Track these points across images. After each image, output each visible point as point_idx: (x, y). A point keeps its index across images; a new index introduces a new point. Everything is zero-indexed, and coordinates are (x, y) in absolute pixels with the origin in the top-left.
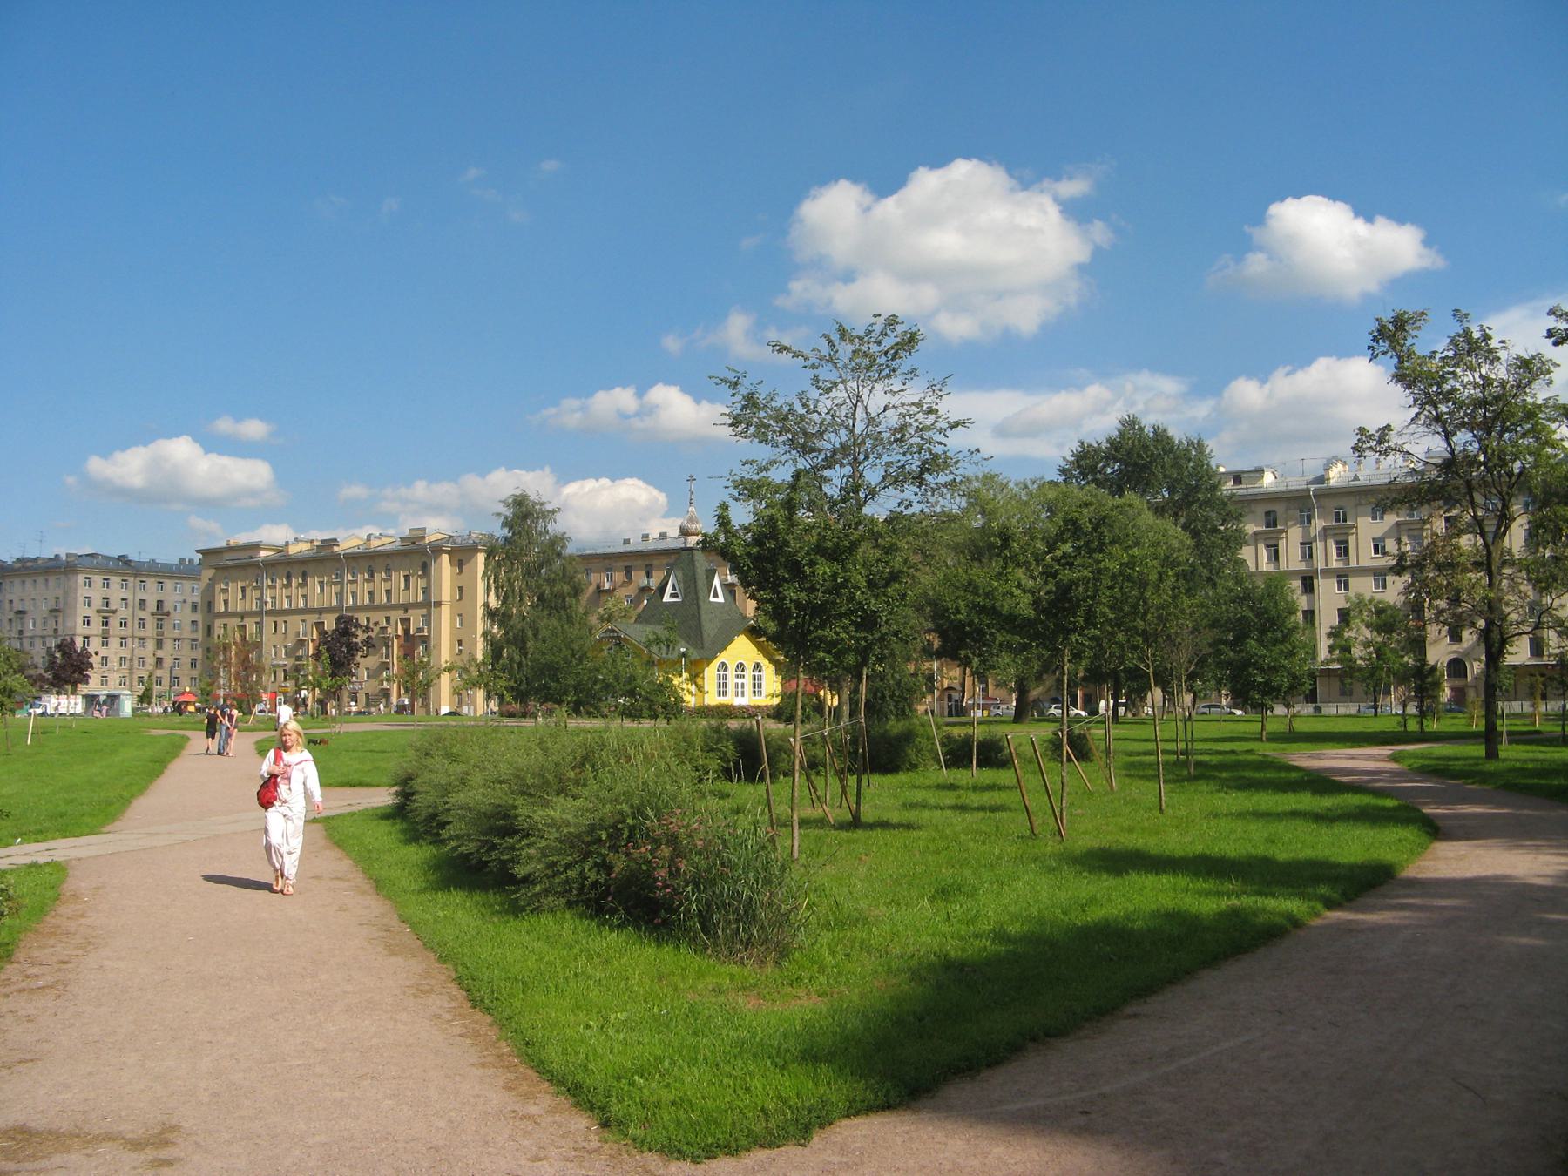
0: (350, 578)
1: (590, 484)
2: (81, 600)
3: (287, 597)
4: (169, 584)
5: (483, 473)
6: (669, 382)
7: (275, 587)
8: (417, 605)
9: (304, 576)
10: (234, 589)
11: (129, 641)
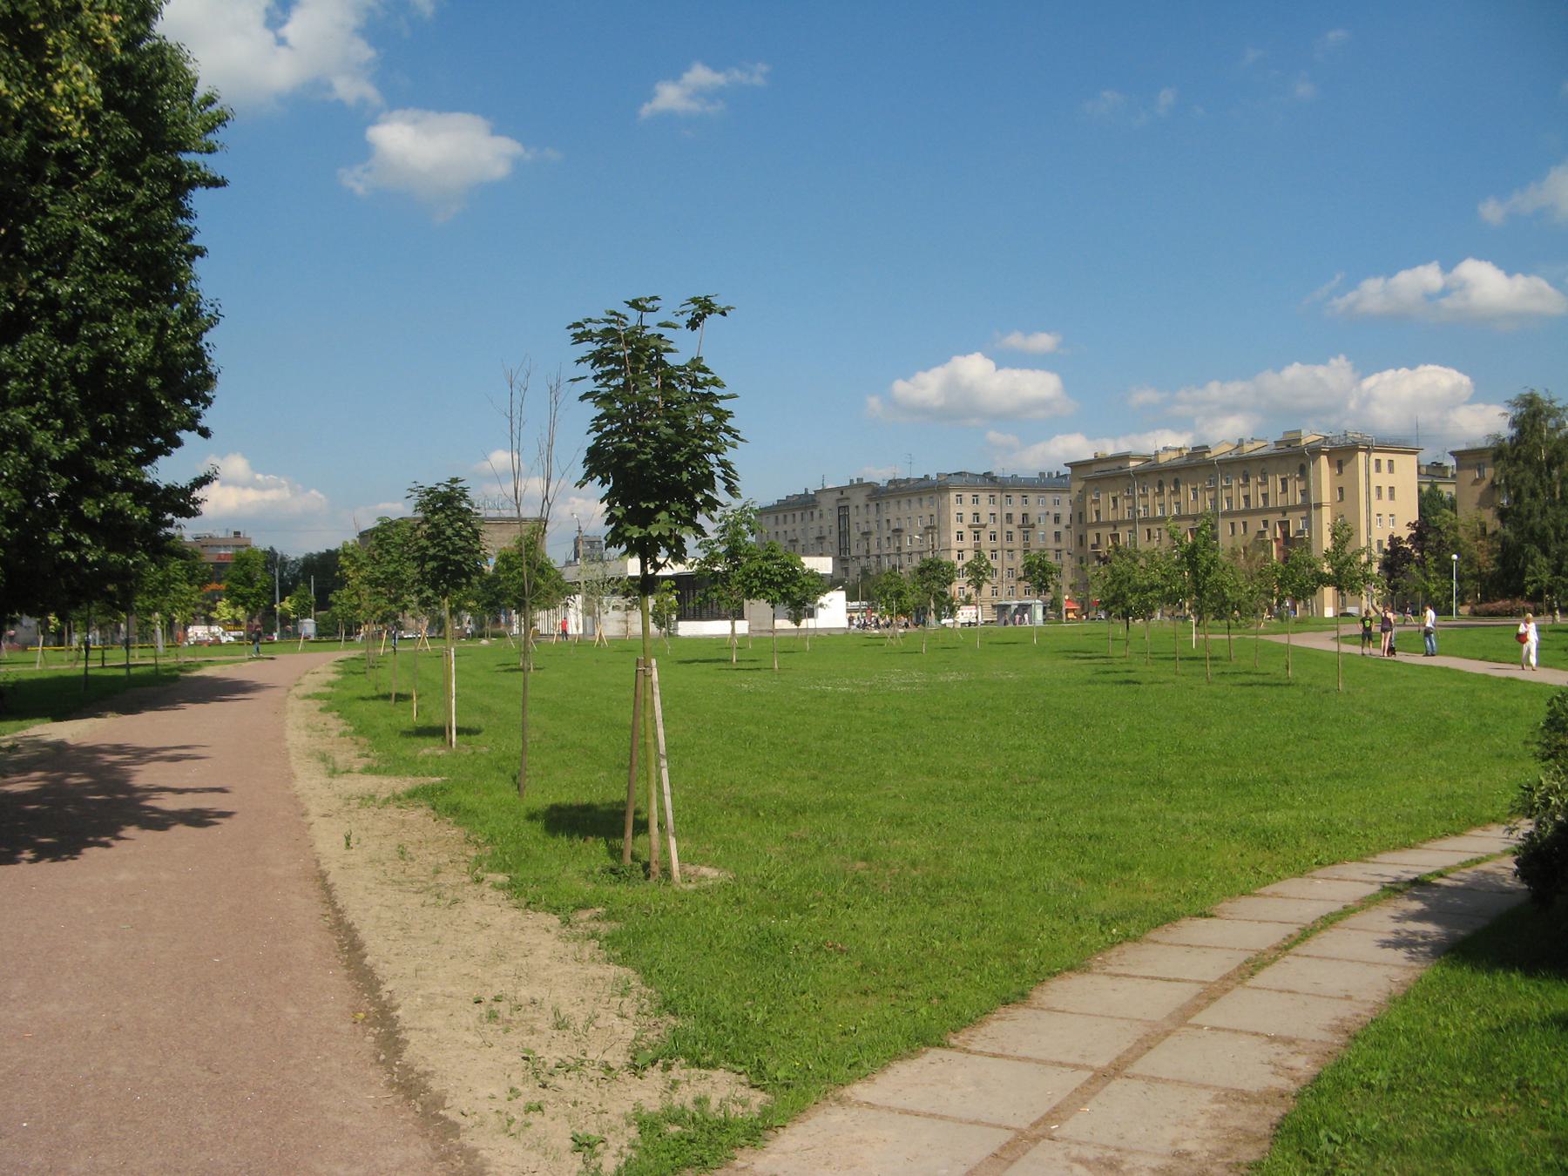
0: (1224, 484)
1: (1389, 374)
2: (954, 516)
3: (1160, 505)
4: (1032, 497)
5: (1279, 369)
6: (1480, 257)
7: (1147, 496)
8: (1295, 508)
9: (1177, 483)
10: (1105, 499)
11: (999, 553)
